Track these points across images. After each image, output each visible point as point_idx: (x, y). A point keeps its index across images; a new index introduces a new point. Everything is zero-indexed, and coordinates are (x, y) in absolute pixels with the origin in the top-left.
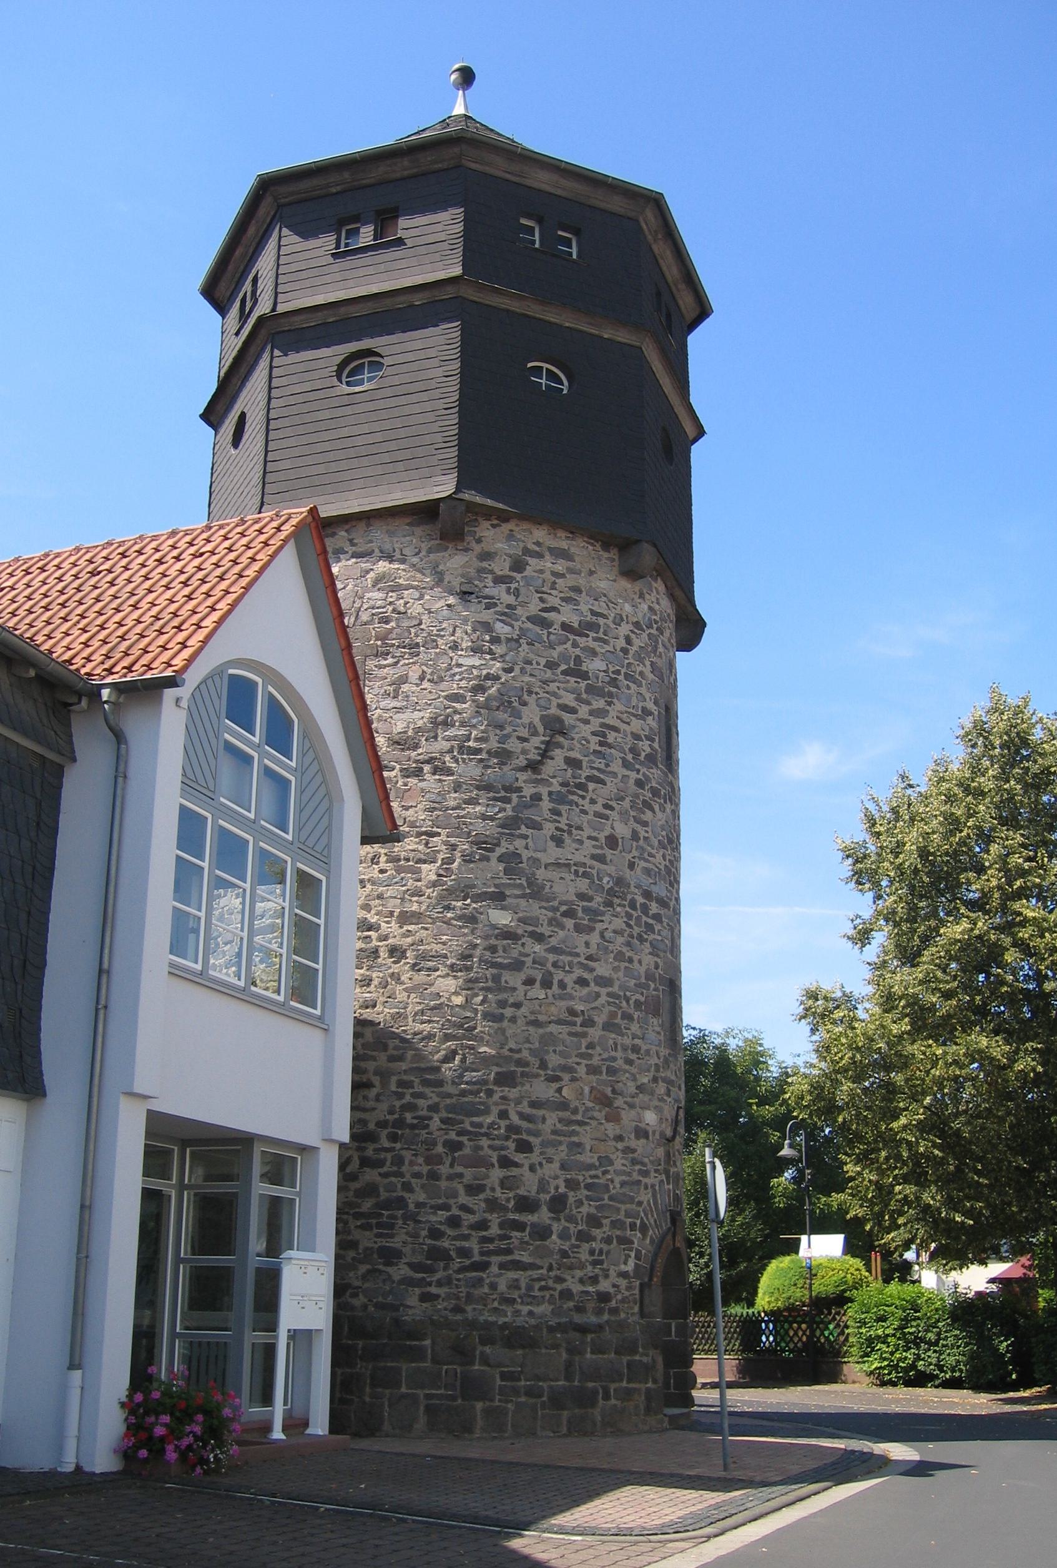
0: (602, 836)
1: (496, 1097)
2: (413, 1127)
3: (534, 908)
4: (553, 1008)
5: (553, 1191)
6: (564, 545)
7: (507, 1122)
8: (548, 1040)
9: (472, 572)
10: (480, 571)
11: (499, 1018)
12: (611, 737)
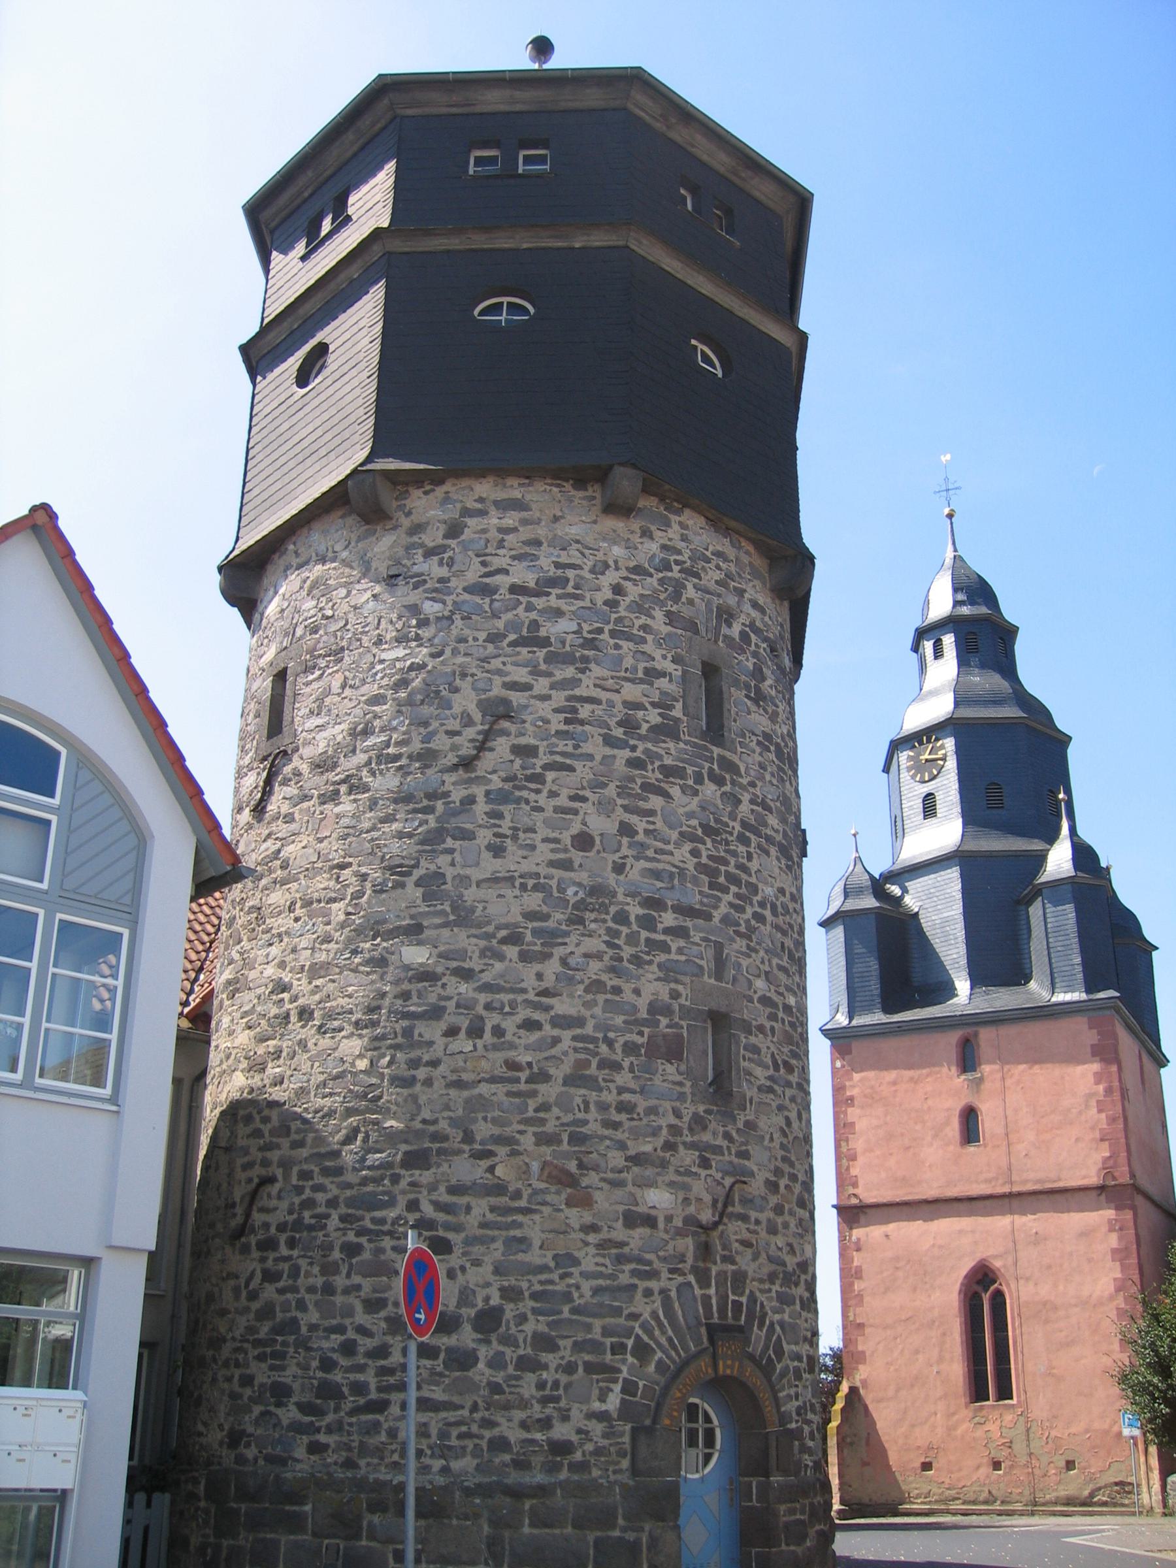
0: (566, 838)
1: (403, 1184)
2: (311, 1228)
3: (462, 939)
4: (483, 1063)
5: (480, 1304)
6: (517, 494)
7: (417, 1215)
8: (478, 1105)
9: (401, 552)
10: (408, 548)
11: (408, 1082)
12: (585, 711)
